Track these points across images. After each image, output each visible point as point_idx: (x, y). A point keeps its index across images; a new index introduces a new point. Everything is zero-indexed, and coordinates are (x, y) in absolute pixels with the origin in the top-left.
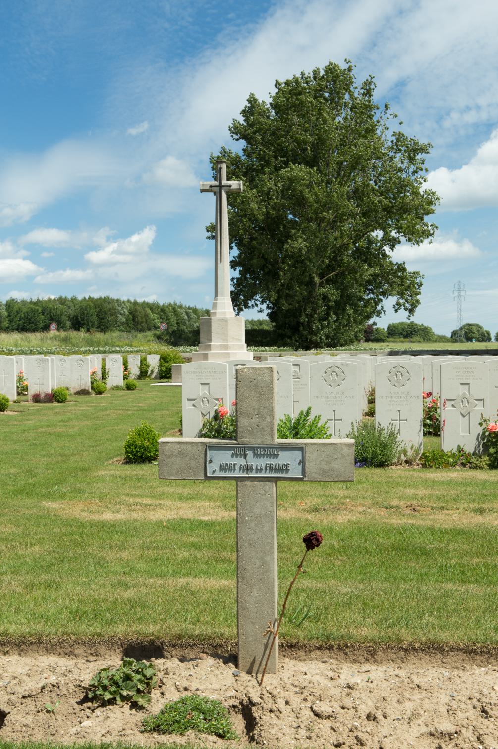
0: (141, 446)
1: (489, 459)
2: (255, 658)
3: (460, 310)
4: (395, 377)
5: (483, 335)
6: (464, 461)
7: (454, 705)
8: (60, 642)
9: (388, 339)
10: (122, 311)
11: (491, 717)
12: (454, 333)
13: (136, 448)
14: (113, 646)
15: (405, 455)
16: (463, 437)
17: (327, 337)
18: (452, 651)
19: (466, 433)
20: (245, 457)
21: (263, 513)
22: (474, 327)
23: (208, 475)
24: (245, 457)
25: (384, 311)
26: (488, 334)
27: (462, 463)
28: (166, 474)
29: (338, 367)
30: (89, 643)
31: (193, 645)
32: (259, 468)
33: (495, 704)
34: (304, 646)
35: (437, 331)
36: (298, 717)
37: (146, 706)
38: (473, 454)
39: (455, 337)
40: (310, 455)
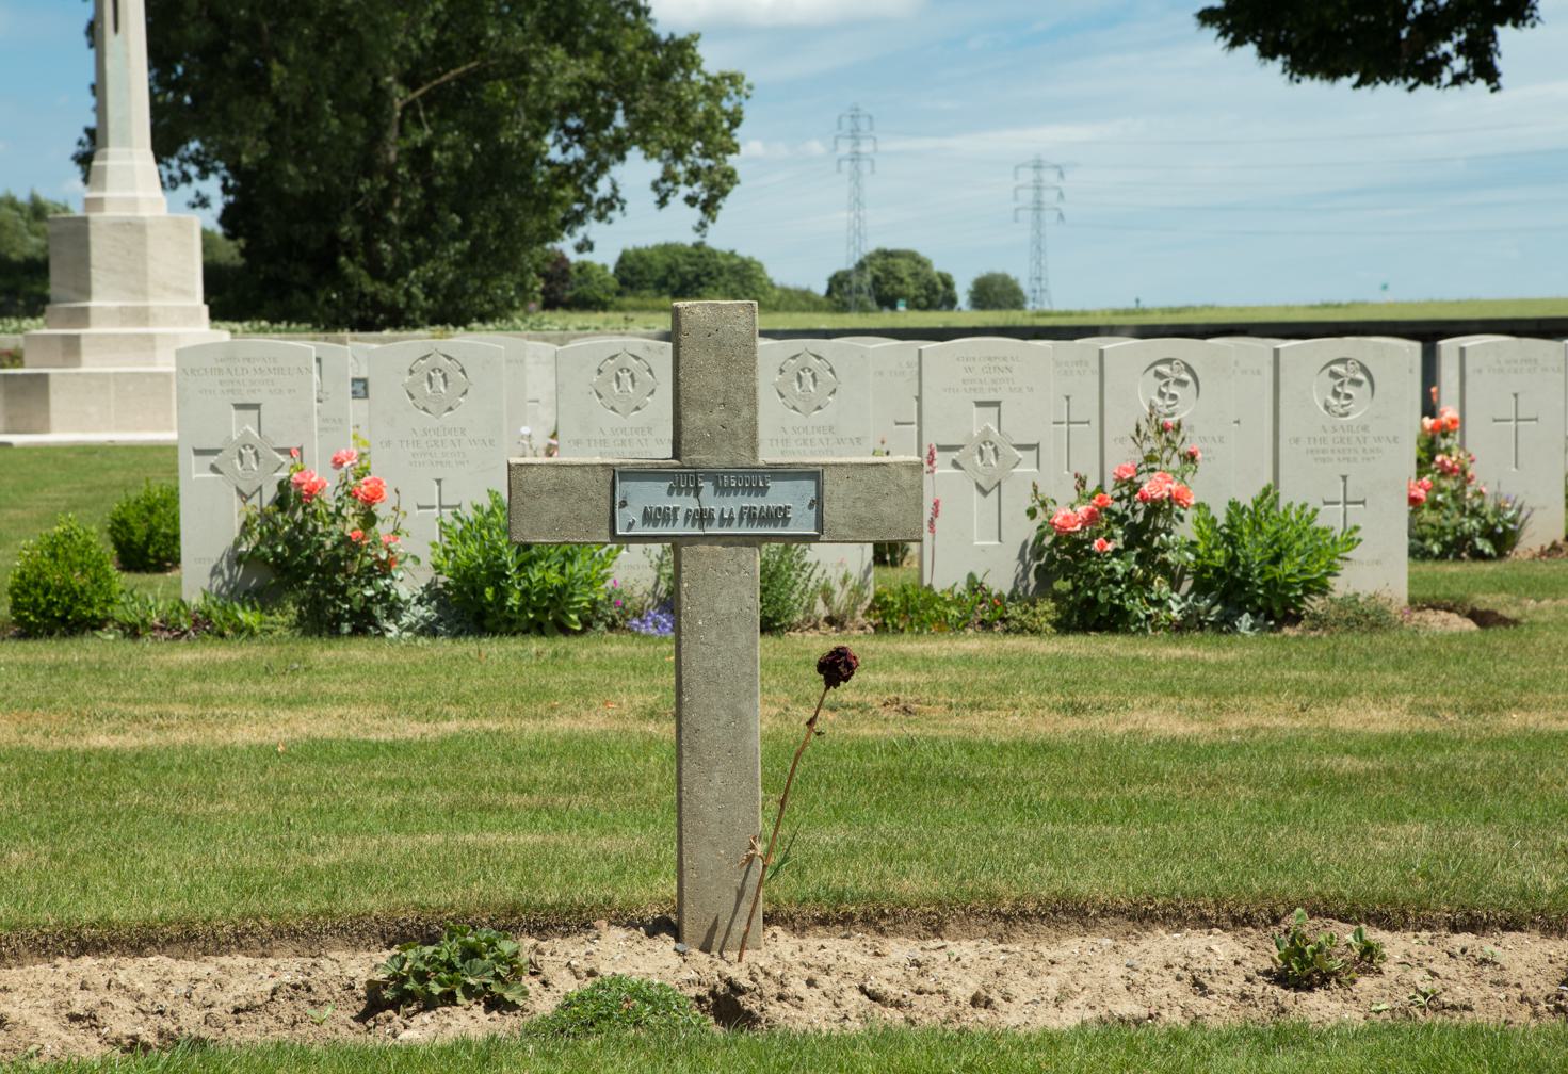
0: (62, 588)
1: (1057, 609)
2: (717, 919)
3: (857, 203)
4: (796, 384)
5: (930, 287)
6: (986, 616)
7: (1137, 977)
8: (236, 936)
9: (617, 300)
11: (1212, 993)
12: (838, 282)
13: (45, 594)
14: (361, 937)
15: (827, 600)
16: (983, 549)
17: (430, 289)
18: (1103, 916)
19: (992, 539)
20: (697, 495)
21: (736, 610)
23: (619, 533)
24: (697, 495)
26: (948, 283)
27: (982, 623)
28: (526, 532)
29: (637, 358)
30: (306, 933)
31: (546, 926)
32: (726, 516)
33: (1218, 971)
34: (791, 917)
35: (783, 272)
36: (837, 1006)
37: (520, 1002)
38: (1011, 598)
39: (841, 292)
40: (834, 488)
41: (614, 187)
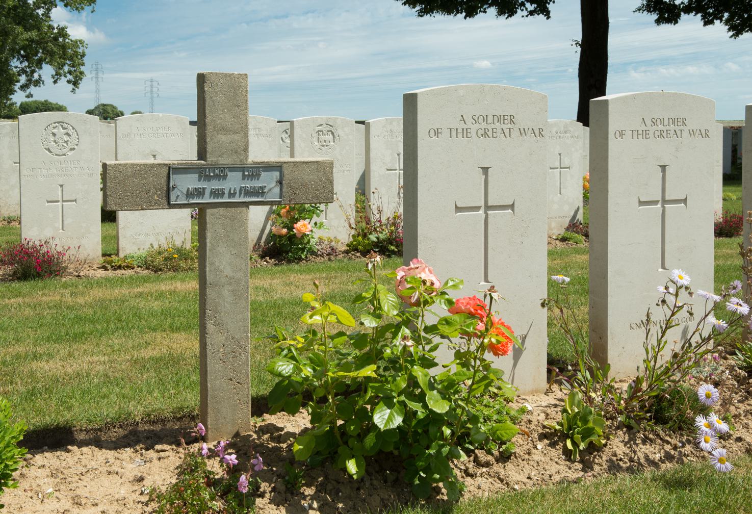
25: (43, 82)
41: (40, 76)
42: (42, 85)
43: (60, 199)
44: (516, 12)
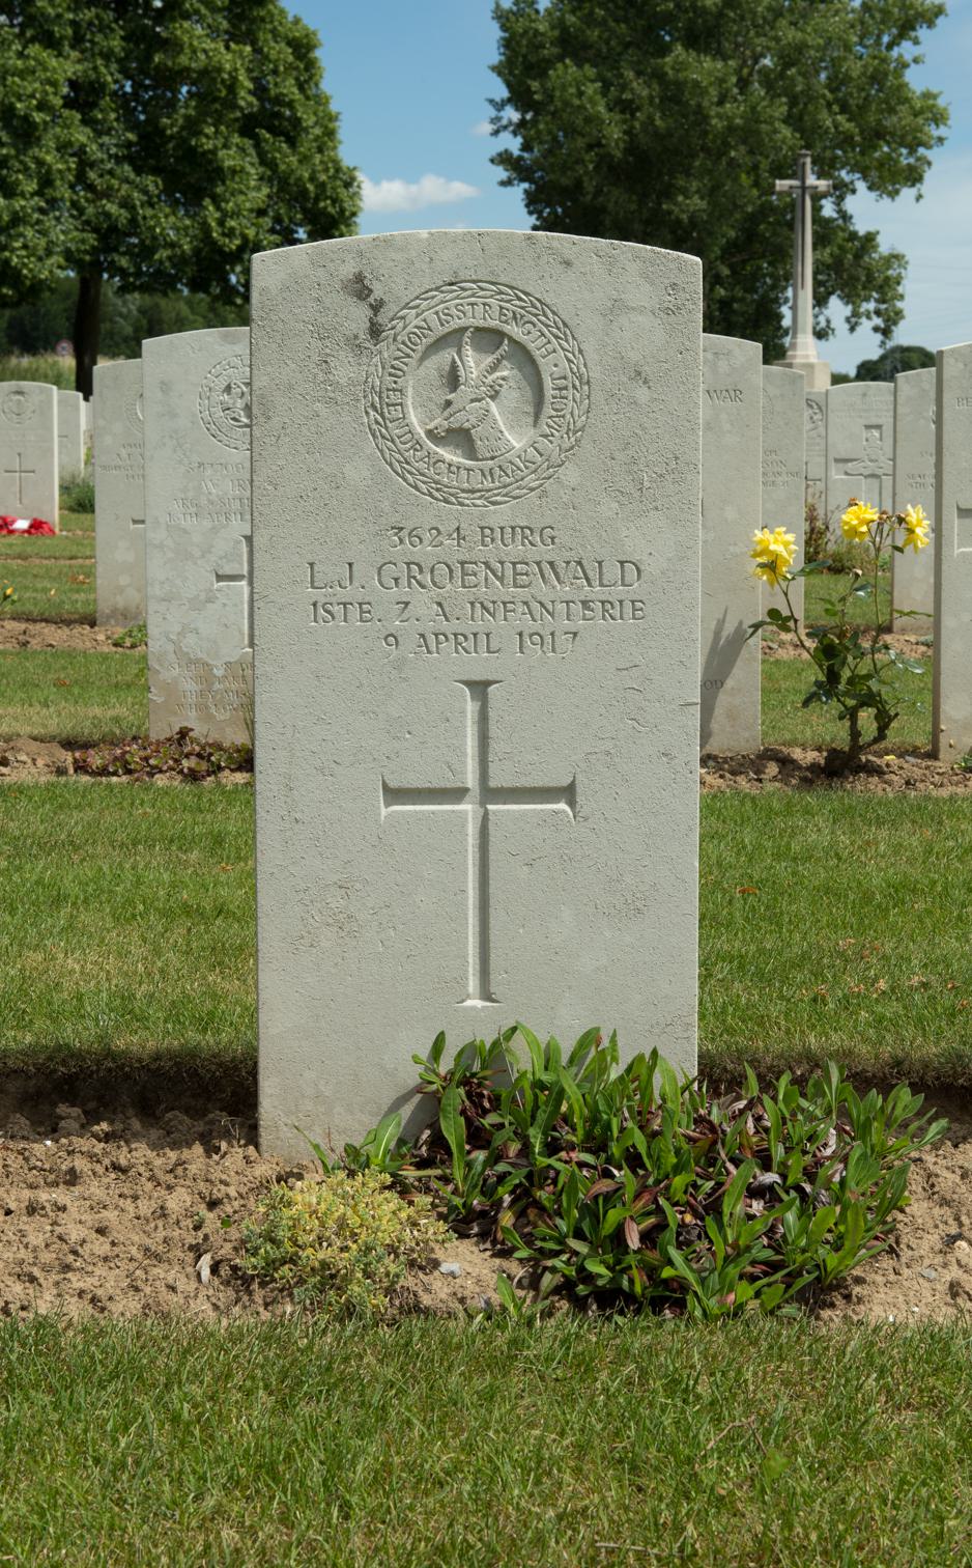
10: (124, 310)
22: (912, 354)
25: (833, 330)
41: (828, 321)
42: (831, 337)
43: (471, 780)
44: (847, 303)
